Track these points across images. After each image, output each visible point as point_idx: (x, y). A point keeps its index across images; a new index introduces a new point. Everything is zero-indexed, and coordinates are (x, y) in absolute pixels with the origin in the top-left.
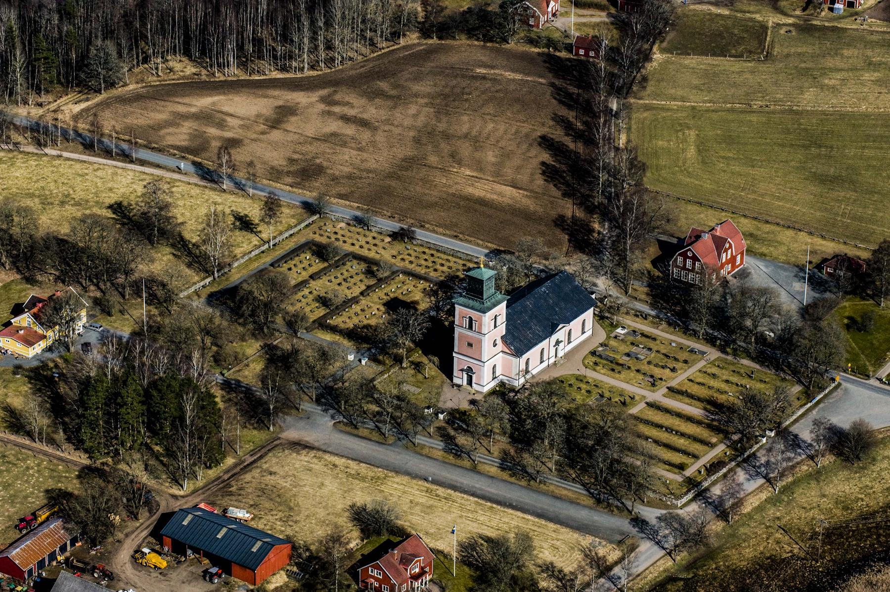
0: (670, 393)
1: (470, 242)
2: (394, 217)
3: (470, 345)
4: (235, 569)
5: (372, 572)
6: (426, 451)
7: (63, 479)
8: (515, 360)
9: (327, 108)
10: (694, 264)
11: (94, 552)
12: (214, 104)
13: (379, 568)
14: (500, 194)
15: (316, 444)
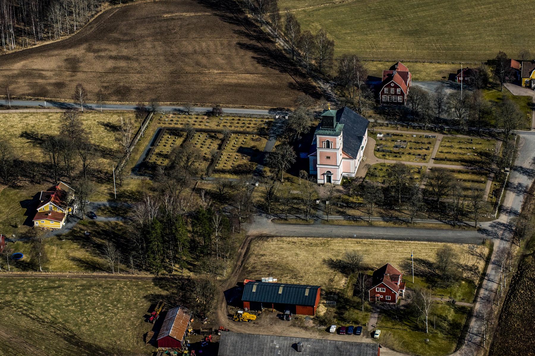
0: (437, 161)
1: (253, 108)
2: (197, 105)
3: (328, 158)
4: (298, 308)
5: (378, 290)
6: (336, 222)
7: (149, 289)
8: (352, 161)
9: (96, 55)
10: (396, 91)
11: (206, 322)
12: (24, 66)
13: (383, 286)
14: (245, 79)
15: (272, 234)
